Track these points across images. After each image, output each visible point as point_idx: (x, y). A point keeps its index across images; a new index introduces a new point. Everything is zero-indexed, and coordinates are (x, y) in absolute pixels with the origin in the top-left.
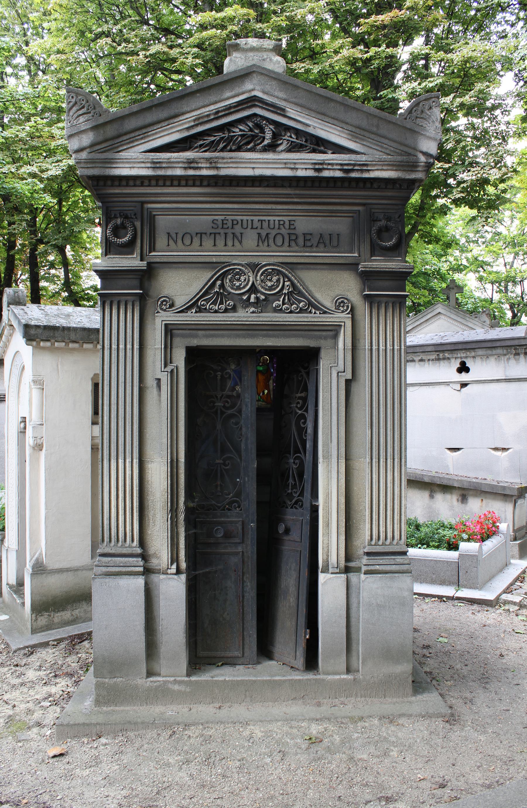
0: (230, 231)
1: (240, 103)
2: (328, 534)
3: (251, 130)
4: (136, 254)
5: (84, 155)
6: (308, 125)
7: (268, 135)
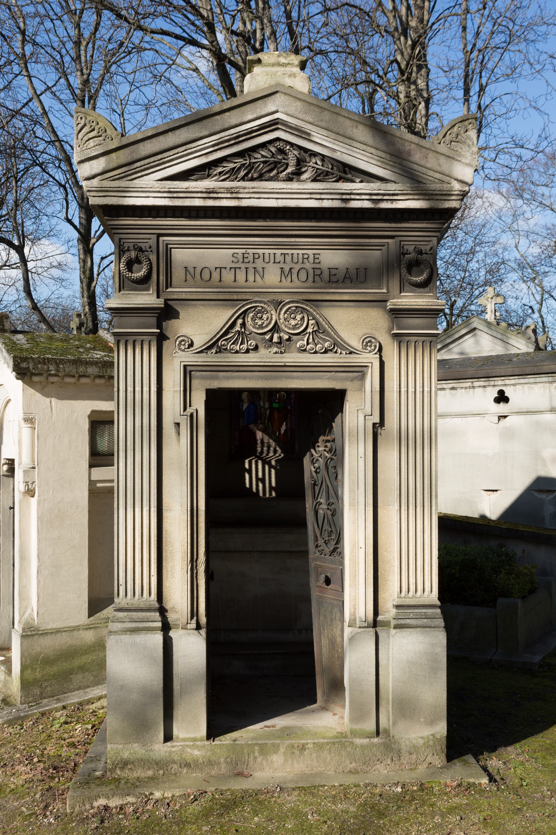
1: (262, 127)
3: (273, 155)
4: (152, 290)
5: (95, 182)
6: (334, 150)
7: (292, 162)
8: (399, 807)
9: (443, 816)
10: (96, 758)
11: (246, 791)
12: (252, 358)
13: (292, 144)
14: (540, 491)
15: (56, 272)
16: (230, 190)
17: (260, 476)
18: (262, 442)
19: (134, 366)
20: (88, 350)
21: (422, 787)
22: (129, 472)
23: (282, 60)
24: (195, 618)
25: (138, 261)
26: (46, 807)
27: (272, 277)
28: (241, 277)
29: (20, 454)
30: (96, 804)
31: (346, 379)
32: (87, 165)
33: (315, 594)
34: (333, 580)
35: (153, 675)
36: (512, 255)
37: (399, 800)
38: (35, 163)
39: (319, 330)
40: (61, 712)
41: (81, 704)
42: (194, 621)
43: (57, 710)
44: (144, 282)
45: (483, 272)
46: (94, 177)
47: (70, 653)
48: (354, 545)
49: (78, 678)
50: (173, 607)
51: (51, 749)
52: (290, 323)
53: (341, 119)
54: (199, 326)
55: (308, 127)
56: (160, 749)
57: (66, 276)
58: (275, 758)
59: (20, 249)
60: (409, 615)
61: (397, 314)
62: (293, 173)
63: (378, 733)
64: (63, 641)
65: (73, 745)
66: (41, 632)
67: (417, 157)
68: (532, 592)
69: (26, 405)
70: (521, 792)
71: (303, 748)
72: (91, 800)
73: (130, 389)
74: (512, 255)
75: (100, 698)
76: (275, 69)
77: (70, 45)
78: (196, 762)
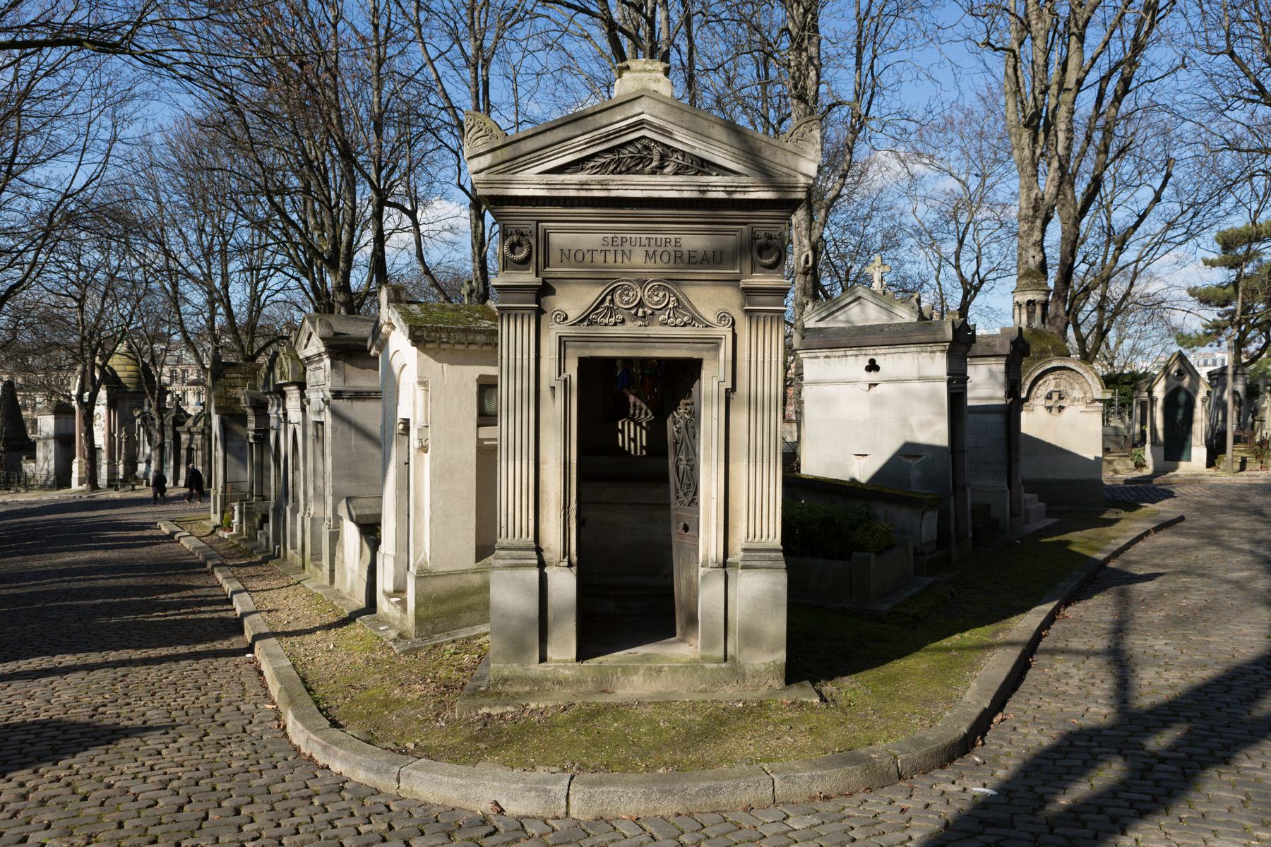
0: (619, 248)
1: (629, 126)
2: (708, 531)
3: (639, 152)
4: (532, 270)
5: (482, 176)
6: (693, 147)
7: (656, 157)
8: (739, 719)
9: (775, 725)
10: (482, 678)
11: (609, 704)
12: (619, 331)
13: (656, 142)
14: (907, 456)
15: (448, 236)
16: (600, 183)
17: (632, 436)
18: (635, 405)
19: (515, 337)
20: (476, 319)
21: (761, 704)
22: (511, 430)
23: (648, 67)
25: (519, 244)
26: (438, 715)
27: (638, 258)
28: (610, 258)
29: (415, 414)
30: (480, 712)
31: (703, 349)
32: (476, 160)
33: (675, 540)
34: (690, 528)
35: (530, 605)
36: (910, 220)
37: (740, 714)
38: (427, 129)
39: (679, 305)
41: (468, 638)
43: (447, 643)
44: (525, 263)
45: (879, 237)
46: (481, 171)
47: (459, 594)
48: (708, 496)
49: (466, 617)
51: (442, 673)
52: (654, 300)
53: (699, 120)
54: (572, 302)
55: (670, 127)
56: (536, 668)
57: (458, 239)
58: (635, 678)
59: (412, 214)
60: (754, 558)
61: (748, 292)
62: (656, 167)
63: (726, 659)
64: (452, 583)
65: (462, 670)
67: (767, 153)
68: (888, 548)
69: (421, 370)
70: (848, 710)
71: (660, 670)
72: (476, 708)
73: (512, 356)
74: (910, 220)
75: (486, 634)
76: (642, 74)
77: (463, 11)
78: (566, 680)
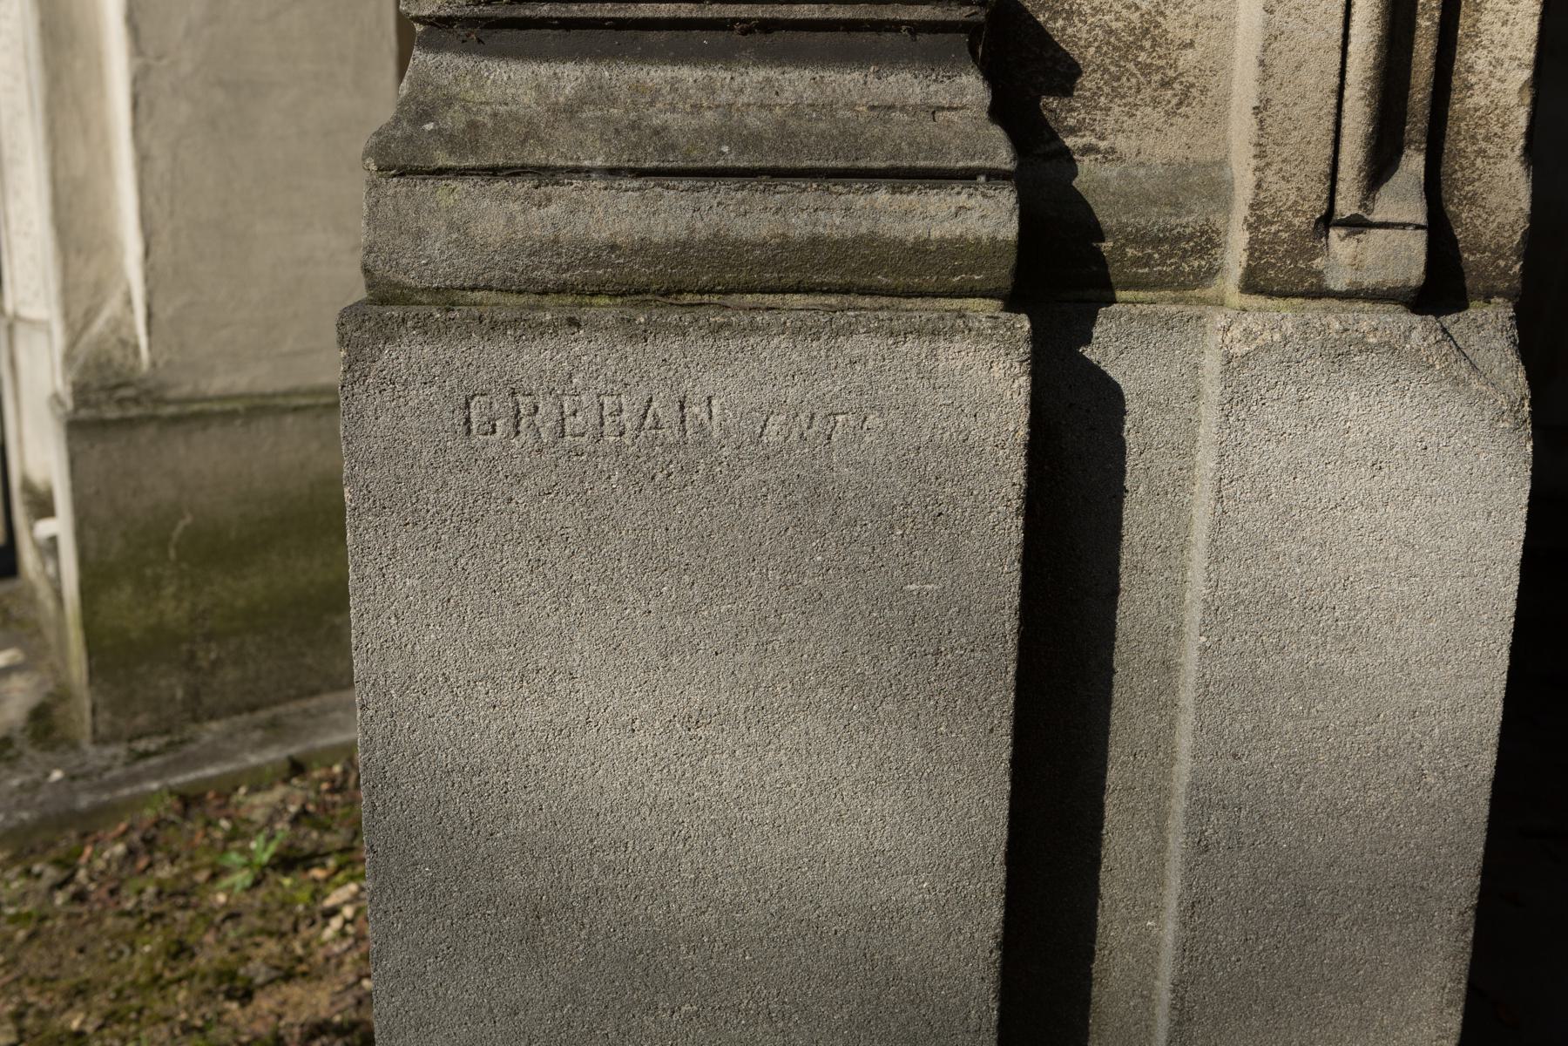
24: (1413, 163)
40: (279, 792)
42: (1402, 200)
50: (1149, 30)
66: (171, 410)
